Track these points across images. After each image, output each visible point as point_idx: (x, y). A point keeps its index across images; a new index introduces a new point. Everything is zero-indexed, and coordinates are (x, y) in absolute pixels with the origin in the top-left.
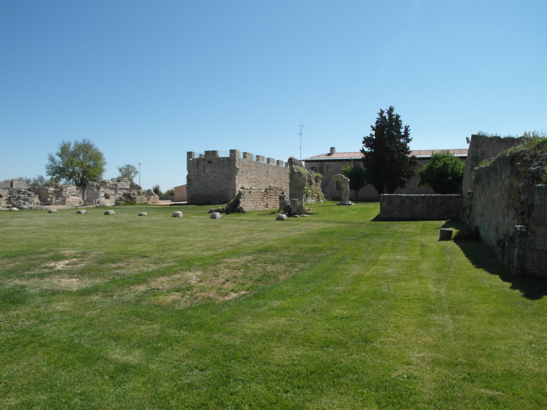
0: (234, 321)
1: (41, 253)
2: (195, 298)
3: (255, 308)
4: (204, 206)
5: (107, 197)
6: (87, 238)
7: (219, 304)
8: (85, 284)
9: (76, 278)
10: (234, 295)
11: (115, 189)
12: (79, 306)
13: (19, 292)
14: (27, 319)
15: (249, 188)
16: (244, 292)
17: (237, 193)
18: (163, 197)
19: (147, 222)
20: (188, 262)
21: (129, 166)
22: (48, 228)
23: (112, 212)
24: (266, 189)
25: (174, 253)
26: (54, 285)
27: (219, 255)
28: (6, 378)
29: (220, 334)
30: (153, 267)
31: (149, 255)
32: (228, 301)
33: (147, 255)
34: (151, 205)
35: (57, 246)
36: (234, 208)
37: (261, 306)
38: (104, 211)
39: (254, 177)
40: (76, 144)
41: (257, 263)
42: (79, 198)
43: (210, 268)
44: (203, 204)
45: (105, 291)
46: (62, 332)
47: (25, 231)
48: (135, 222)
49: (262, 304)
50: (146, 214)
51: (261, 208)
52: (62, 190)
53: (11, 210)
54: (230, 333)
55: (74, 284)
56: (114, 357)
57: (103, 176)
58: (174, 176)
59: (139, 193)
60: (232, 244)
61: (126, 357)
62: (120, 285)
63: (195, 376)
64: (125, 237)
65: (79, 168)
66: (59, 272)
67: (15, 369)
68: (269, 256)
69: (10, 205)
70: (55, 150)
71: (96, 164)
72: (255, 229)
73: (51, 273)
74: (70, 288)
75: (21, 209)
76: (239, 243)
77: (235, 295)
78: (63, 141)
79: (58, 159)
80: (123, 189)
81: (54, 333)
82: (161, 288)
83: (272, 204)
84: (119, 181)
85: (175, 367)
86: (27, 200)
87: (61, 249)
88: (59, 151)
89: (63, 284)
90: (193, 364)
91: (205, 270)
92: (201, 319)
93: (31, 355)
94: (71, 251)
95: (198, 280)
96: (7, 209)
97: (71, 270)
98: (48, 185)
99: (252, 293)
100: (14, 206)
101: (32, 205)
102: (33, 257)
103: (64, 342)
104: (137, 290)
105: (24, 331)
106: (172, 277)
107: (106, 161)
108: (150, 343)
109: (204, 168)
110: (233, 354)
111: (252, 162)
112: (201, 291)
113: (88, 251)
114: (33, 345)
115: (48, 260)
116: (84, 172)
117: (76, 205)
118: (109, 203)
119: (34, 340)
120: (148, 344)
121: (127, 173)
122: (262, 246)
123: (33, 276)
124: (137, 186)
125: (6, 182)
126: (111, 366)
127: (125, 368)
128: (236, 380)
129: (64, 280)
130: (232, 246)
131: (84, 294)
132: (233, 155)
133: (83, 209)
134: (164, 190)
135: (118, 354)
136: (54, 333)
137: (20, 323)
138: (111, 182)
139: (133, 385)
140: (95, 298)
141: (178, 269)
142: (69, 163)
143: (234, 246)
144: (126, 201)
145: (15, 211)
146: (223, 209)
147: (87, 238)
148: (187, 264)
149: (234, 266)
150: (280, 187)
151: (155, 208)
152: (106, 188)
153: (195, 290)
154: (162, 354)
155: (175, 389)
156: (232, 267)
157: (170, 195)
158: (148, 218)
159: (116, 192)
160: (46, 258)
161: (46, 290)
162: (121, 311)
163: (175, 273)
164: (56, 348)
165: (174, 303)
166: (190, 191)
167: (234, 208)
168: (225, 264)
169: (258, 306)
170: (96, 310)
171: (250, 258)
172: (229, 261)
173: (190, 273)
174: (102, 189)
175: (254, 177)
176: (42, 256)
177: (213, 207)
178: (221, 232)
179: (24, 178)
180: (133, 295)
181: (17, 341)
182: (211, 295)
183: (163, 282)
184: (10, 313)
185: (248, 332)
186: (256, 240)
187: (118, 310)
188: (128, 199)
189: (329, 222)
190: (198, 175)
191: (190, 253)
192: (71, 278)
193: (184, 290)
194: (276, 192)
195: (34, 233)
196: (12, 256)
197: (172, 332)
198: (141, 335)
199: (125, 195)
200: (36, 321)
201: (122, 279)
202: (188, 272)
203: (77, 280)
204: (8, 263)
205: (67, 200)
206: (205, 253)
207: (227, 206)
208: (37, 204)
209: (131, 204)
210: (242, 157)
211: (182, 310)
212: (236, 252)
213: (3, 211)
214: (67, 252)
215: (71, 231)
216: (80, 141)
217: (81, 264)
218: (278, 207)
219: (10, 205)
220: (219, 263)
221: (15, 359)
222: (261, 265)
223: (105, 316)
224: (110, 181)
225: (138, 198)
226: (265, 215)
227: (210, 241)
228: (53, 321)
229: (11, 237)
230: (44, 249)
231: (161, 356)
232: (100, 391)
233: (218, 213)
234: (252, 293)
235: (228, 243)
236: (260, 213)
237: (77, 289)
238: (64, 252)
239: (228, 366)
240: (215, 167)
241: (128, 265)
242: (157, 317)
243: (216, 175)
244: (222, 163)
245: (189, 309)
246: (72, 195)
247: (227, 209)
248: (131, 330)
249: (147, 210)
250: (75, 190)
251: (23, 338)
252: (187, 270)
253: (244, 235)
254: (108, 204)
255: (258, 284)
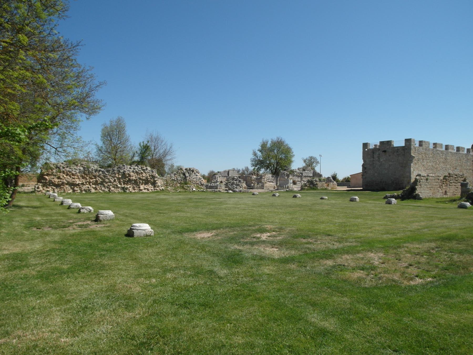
0: (423, 308)
1: (250, 226)
2: (380, 278)
3: (446, 298)
4: (378, 192)
5: (294, 183)
6: (281, 216)
7: (405, 288)
8: (284, 253)
9: (276, 248)
10: (418, 281)
11: (301, 177)
12: (281, 272)
13: (238, 255)
15: (426, 175)
17: (413, 180)
19: (328, 205)
20: (369, 243)
21: (311, 158)
22: (253, 207)
23: (299, 195)
24: (445, 176)
25: (355, 234)
28: (234, 320)
29: (411, 318)
30: (337, 245)
31: (333, 234)
32: (414, 285)
33: (331, 234)
34: (330, 190)
35: (261, 221)
36: (410, 194)
37: (453, 297)
39: (430, 164)
40: (272, 142)
42: (273, 184)
43: (391, 251)
44: (377, 190)
46: (270, 291)
47: (238, 208)
48: (318, 204)
49: (454, 295)
50: (327, 198)
51: (439, 195)
52: (261, 178)
53: (228, 192)
54: (421, 319)
55: (275, 252)
57: (292, 166)
58: (349, 164)
59: (320, 180)
60: (411, 229)
61: (323, 323)
62: (311, 258)
64: (311, 217)
65: (274, 160)
68: (454, 244)
69: (227, 189)
70: (257, 147)
71: (286, 157)
72: (435, 216)
74: (273, 256)
75: (234, 191)
76: (418, 229)
77: (420, 281)
78: (263, 140)
79: (259, 154)
80: (307, 176)
81: (265, 291)
82: (346, 264)
84: (304, 170)
85: (369, 342)
86: (238, 185)
87: (264, 223)
88: (260, 148)
91: (386, 253)
92: (388, 300)
94: (271, 226)
95: (381, 261)
97: (273, 242)
98: (252, 174)
99: (441, 282)
100: (230, 189)
102: (245, 228)
103: (273, 300)
104: (325, 264)
105: (243, 285)
106: (355, 256)
107: (294, 154)
108: (343, 314)
109: (379, 158)
110: (428, 342)
111: (429, 150)
112: (385, 272)
113: (283, 227)
115: (256, 232)
118: (296, 188)
121: (310, 163)
123: (246, 243)
124: (318, 174)
125: (225, 172)
126: (311, 328)
127: (323, 332)
129: (267, 249)
130: (411, 231)
132: (408, 144)
134: (340, 177)
135: (315, 318)
136: (265, 291)
137: (240, 279)
138: (298, 171)
140: (293, 266)
141: (361, 249)
142: (267, 157)
145: (231, 193)
146: (398, 195)
148: (369, 245)
149: (416, 251)
150: (461, 174)
152: (294, 176)
153: (379, 270)
154: (355, 327)
156: (414, 253)
157: (346, 182)
158: (328, 202)
159: (301, 179)
160: (254, 230)
161: (256, 255)
162: (315, 281)
163: (358, 253)
164: (267, 303)
165: (360, 280)
166: (366, 178)
167: (410, 194)
168: (406, 249)
169: (449, 296)
170: (294, 276)
171: (433, 245)
172: (411, 246)
173: (372, 254)
174: (291, 177)
175: (430, 164)
176: (250, 228)
177: (388, 194)
179: (236, 169)
180: (322, 268)
181: (240, 293)
182: (396, 278)
183: (346, 259)
184: (234, 270)
185: (442, 321)
186: (437, 227)
188: (311, 185)
189: (419, 206)
190: (373, 163)
191: (370, 235)
192: (273, 247)
194: (457, 179)
197: (362, 307)
198: (334, 306)
199: (308, 181)
202: (370, 253)
203: (277, 249)
204: (229, 232)
205: (265, 185)
206: (385, 236)
207: (403, 193)
208: (245, 188)
209: (314, 189)
210: (417, 145)
211: (368, 288)
212: (416, 237)
213: (223, 193)
215: (270, 210)
216: (275, 139)
217: (279, 237)
218: (458, 195)
219: (227, 189)
220: (399, 247)
222: (446, 253)
223: (302, 283)
224: (184, 169)
225: (319, 184)
226: (444, 202)
228: (262, 280)
229: (230, 212)
230: (252, 223)
231: (354, 329)
233: (394, 199)
234: (441, 282)
236: (438, 200)
237: (278, 257)
238: (266, 226)
240: (390, 156)
241: (316, 241)
242: (346, 291)
243: (391, 163)
244: (397, 152)
245: (376, 287)
246: (269, 182)
247: (402, 196)
248: (325, 299)
249: (327, 194)
251: (243, 291)
252: (368, 251)
253: (423, 221)
254: (295, 189)
255: (446, 273)
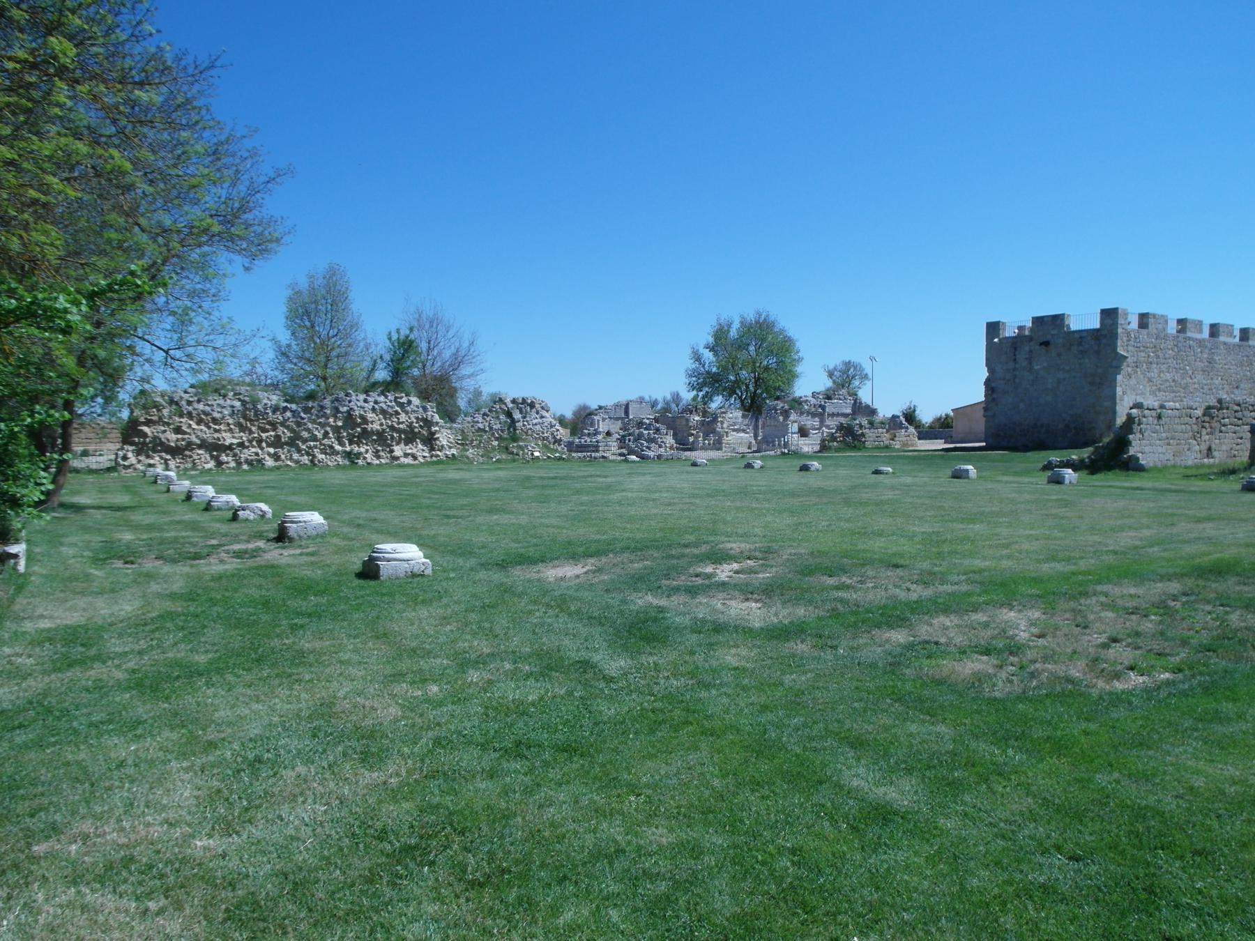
0: (1149, 748)
1: (686, 546)
2: (1033, 675)
4: (1029, 454)
5: (803, 432)
6: (769, 518)
7: (1101, 697)
8: (776, 615)
9: (757, 601)
10: (1136, 680)
11: (821, 416)
12: (769, 662)
13: (655, 620)
14: (675, 676)
15: (1156, 404)
16: (1167, 675)
17: (1120, 420)
18: (927, 433)
19: (893, 488)
21: (848, 364)
22: (694, 496)
23: (816, 464)
24: (1209, 408)
25: (967, 562)
26: (714, 610)
27: (1088, 573)
29: (1116, 775)
32: (1123, 692)
33: (902, 562)
34: (898, 450)
35: (714, 533)
36: (1113, 456)
38: (799, 463)
39: (1168, 376)
41: (1195, 601)
42: (748, 437)
43: (1063, 605)
44: (1026, 448)
45: (823, 640)
46: (742, 710)
47: (654, 500)
50: (890, 469)
51: (1192, 457)
52: (715, 420)
53: (626, 461)
55: (753, 612)
56: (855, 783)
57: (795, 389)
59: (871, 423)
62: (849, 626)
63: (1057, 870)
64: (848, 520)
65: (749, 373)
66: (724, 584)
67: (663, 772)
68: (1230, 585)
69: (624, 451)
72: (1180, 511)
73: (708, 586)
75: (643, 457)
76: (1136, 548)
77: (1141, 679)
79: (708, 356)
80: (838, 415)
81: (727, 711)
82: (943, 640)
83: (1224, 447)
84: (829, 398)
85: (1003, 837)
86: (653, 440)
87: (723, 538)
89: (733, 612)
90: (1049, 837)
91: (1050, 610)
92: (1055, 729)
93: (689, 749)
94: (743, 545)
95: (1035, 630)
96: (619, 458)
98: (689, 410)
99: (1195, 682)
100: (631, 452)
101: (662, 450)
104: (887, 641)
105: (669, 697)
106: (966, 618)
107: (801, 354)
108: (934, 767)
109: (1030, 360)
110: (1161, 834)
111: (1166, 337)
112: (1046, 659)
113: (775, 546)
114: (691, 728)
115: (701, 561)
116: (757, 381)
117: (741, 450)
118: (808, 445)
119: (691, 719)
120: (929, 767)
121: (846, 378)
122: (1206, 559)
123: (676, 590)
124: (868, 407)
125: (617, 406)
126: (851, 802)
127: (883, 814)
128: (1177, 907)
129: (733, 603)
130: (1115, 553)
131: (778, 637)
132: (1109, 322)
133: (757, 458)
134: (926, 416)
135: (860, 777)
136: (727, 711)
137: (662, 682)
138: (813, 401)
139: (904, 858)
140: (801, 648)
142: (731, 364)
143: (1124, 553)
144: (844, 441)
145: (634, 462)
146: (1082, 461)
147: (769, 518)
148: (1004, 590)
149: (1130, 604)
151: (908, 457)
152: (802, 413)
153: (1030, 654)
154: (967, 798)
155: (1011, 889)
156: (1125, 608)
157: (942, 427)
158: (895, 481)
159: (822, 422)
160: (697, 556)
161: (704, 621)
163: (975, 610)
164: (733, 742)
165: (979, 680)
166: (994, 416)
167: (1113, 456)
168: (1103, 599)
169: (1218, 717)
170: (805, 673)
171: (1175, 587)
173: (1012, 614)
174: (793, 417)
175: (1168, 376)
177: (1055, 457)
178: (1081, 517)
179: (647, 398)
180: (879, 650)
182: (1075, 673)
183: (943, 627)
185: (1199, 782)
186: (1185, 542)
187: (851, 679)
190: (1015, 376)
191: (1005, 563)
192: (747, 600)
193: (999, 652)
195: (669, 504)
196: (637, 548)
197: (984, 748)
198: (911, 746)
199: (841, 427)
200: (691, 682)
201: (852, 613)
202: (1005, 611)
203: (759, 605)
206: (1046, 567)
208: (671, 448)
209: (855, 448)
210: (1134, 325)
212: (1129, 568)
213: (613, 461)
214: (734, 545)
215: (738, 504)
216: (751, 316)
217: (763, 572)
219: (624, 451)
220: (1085, 594)
221: (662, 752)
222: (1208, 608)
223: (826, 689)
225: (870, 434)
227: (1055, 539)
230: (692, 538)
231: (964, 803)
232: (834, 855)
233: (1070, 471)
235: (1106, 545)
236: (1189, 472)
237: (762, 625)
238: (729, 546)
239: (1148, 864)
240: (1059, 355)
241: (861, 582)
242: (942, 707)
244: (1080, 344)
245: (1022, 697)
246: (734, 430)
247: (1093, 462)
248: (886, 729)
249: (890, 460)
250: (740, 420)
251: (671, 711)
252: (1002, 605)
253: (1148, 527)
254: (806, 449)
255: (1210, 658)
